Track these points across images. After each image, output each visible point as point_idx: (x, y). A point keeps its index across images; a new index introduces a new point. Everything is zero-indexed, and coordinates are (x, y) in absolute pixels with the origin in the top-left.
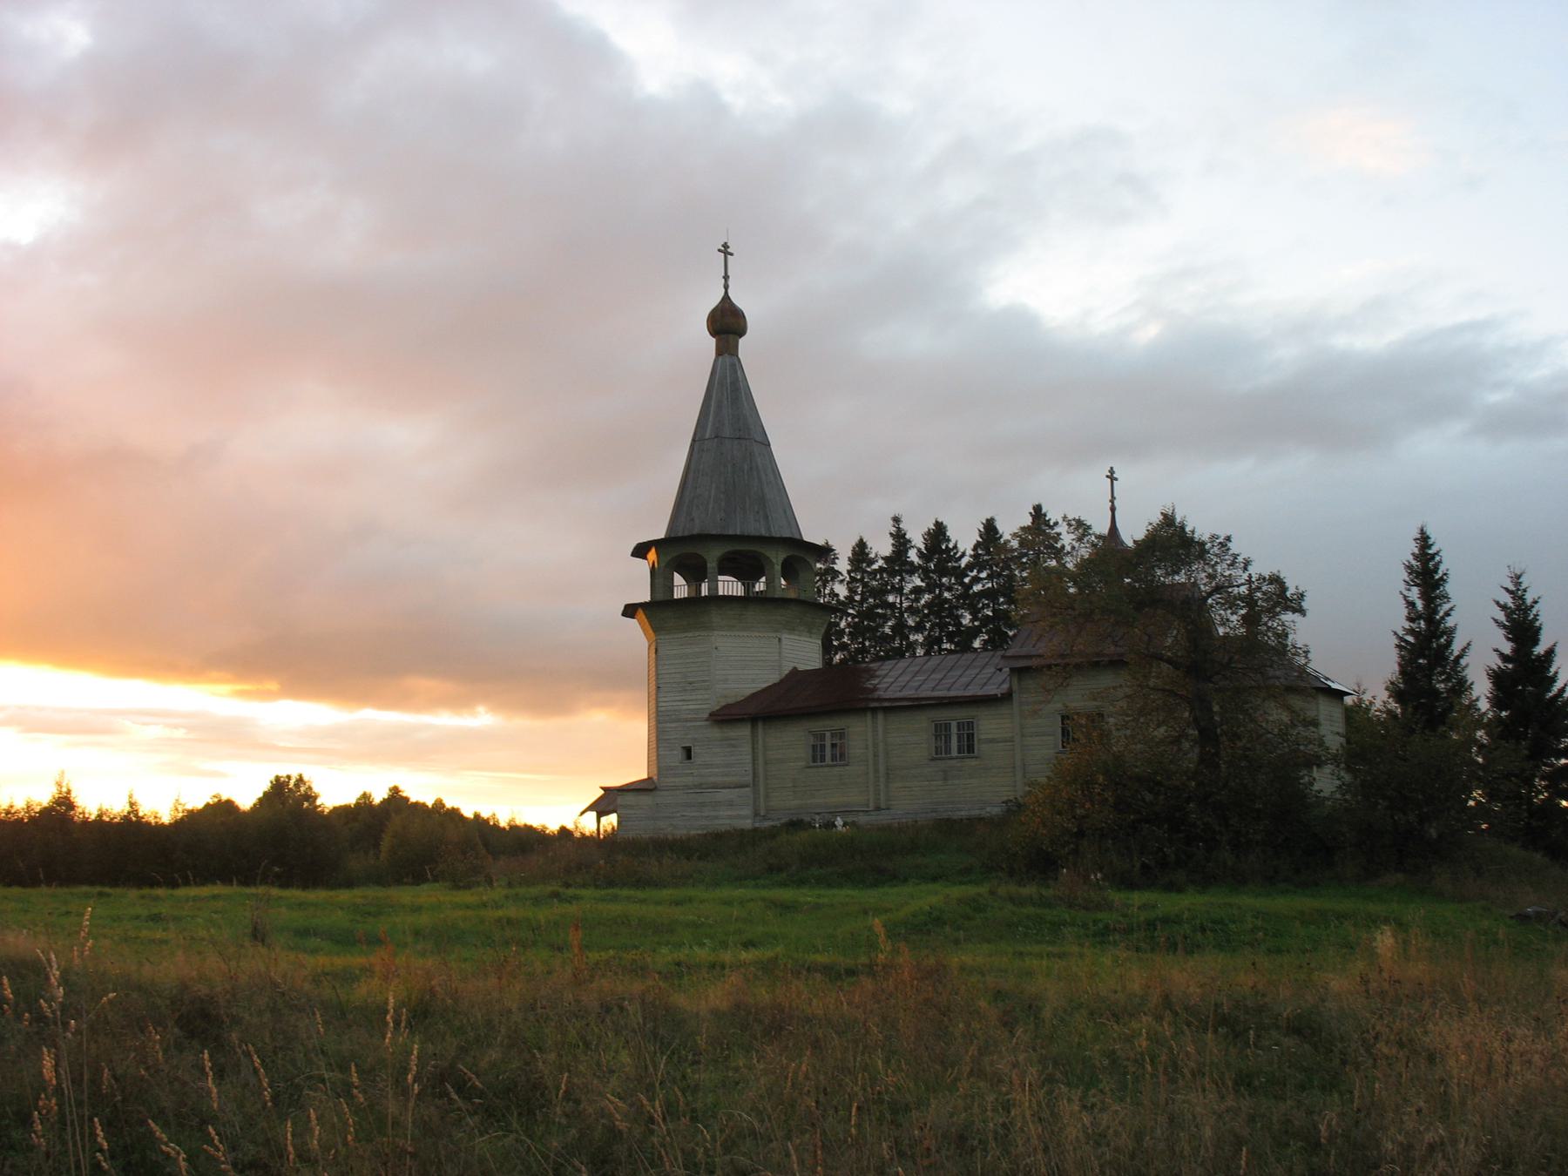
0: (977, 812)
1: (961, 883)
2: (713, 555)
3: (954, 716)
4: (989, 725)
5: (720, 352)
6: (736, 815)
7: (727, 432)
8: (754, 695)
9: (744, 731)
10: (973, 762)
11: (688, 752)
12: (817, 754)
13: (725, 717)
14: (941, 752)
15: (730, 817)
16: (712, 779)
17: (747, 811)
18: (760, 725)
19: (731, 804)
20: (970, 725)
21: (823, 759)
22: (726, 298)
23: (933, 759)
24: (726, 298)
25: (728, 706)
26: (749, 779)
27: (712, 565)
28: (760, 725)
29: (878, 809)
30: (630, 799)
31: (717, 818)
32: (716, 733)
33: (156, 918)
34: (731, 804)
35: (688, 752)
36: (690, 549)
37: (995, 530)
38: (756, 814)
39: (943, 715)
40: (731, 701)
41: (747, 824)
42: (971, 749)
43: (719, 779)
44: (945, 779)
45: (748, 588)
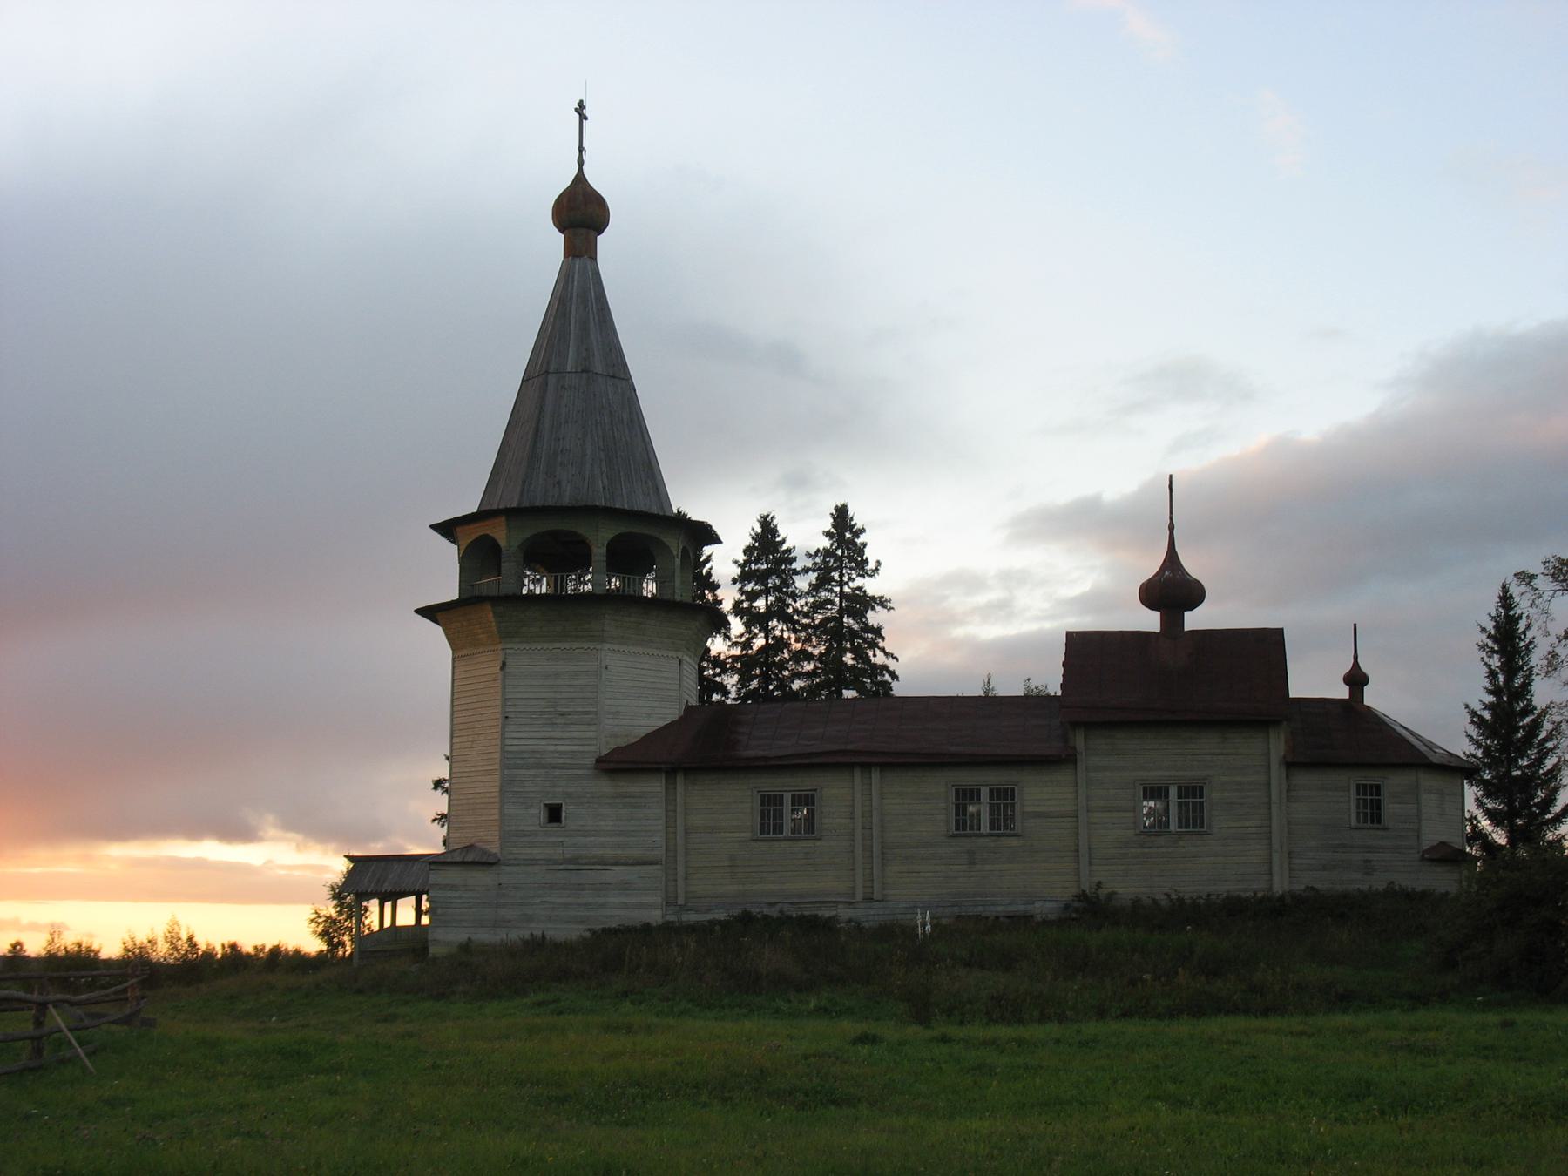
0: (1022, 908)
1: (1199, 1008)
2: (600, 538)
3: (986, 780)
4: (1040, 794)
5: (571, 251)
6: (635, 901)
7: (599, 367)
8: (648, 735)
9: (655, 786)
10: (1015, 842)
11: (554, 814)
12: (769, 823)
13: (620, 764)
14: (963, 824)
15: (625, 906)
16: (599, 852)
17: (657, 899)
18: (680, 779)
19: (625, 887)
20: (1377, 789)
21: (779, 829)
22: (580, 179)
23: (954, 836)
24: (580, 179)
25: (618, 750)
26: (660, 853)
27: (599, 552)
28: (680, 779)
29: (869, 899)
30: (452, 876)
31: (603, 906)
32: (604, 786)
33: (791, 1038)
34: (625, 887)
35: (554, 814)
36: (637, 529)
37: (774, 532)
38: (670, 902)
39: (968, 778)
40: (622, 742)
41: (655, 917)
42: (1199, 821)
43: (609, 853)
44: (972, 863)
45: (558, 584)
